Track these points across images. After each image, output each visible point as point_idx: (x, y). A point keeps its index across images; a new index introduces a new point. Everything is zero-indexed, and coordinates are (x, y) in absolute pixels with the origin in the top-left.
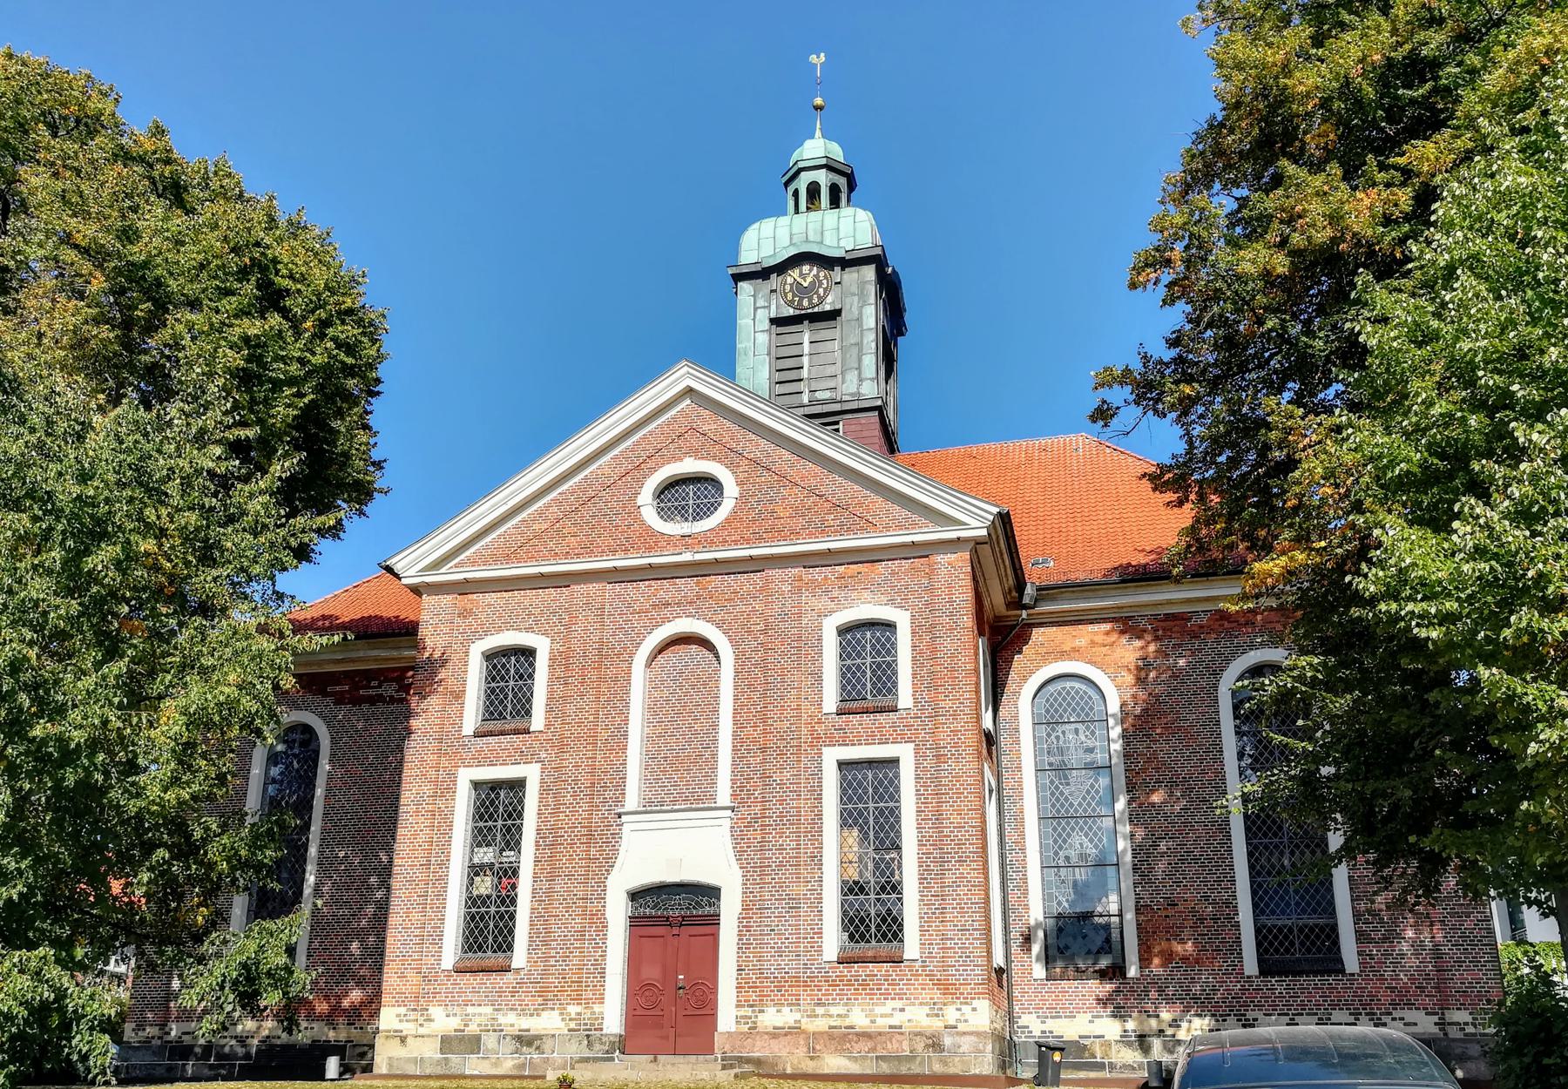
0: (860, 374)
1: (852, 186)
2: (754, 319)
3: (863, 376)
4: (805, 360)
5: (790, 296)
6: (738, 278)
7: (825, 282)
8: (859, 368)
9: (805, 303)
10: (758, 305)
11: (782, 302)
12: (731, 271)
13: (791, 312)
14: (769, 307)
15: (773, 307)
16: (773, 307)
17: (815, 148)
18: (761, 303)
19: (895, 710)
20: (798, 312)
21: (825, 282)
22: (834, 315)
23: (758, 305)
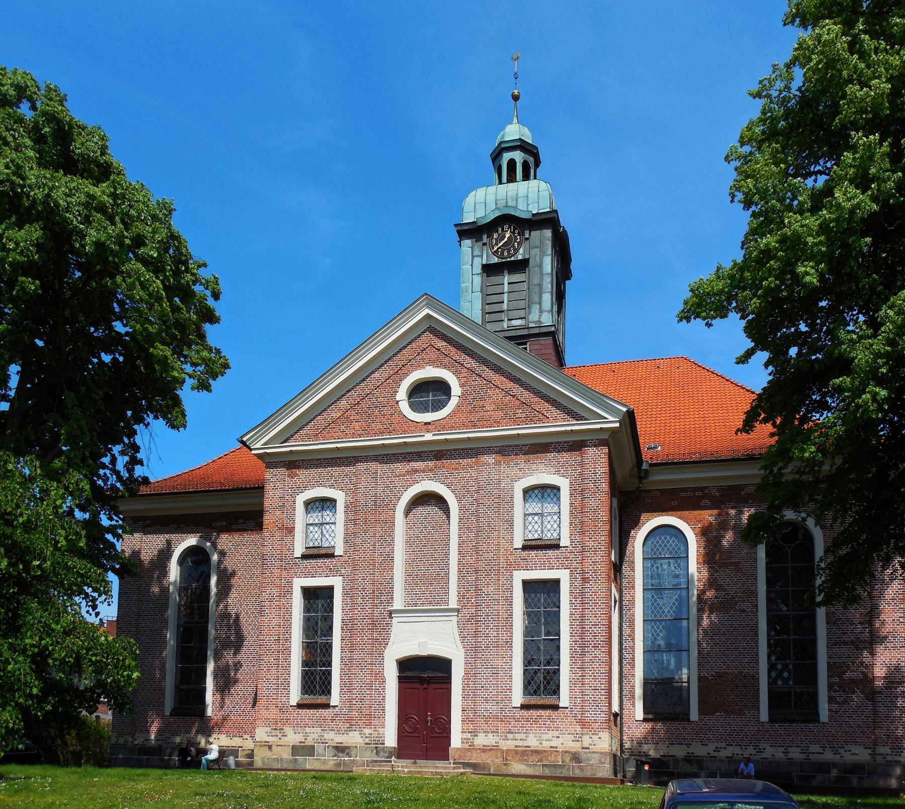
2: (472, 265)
9: (506, 254)
14: (482, 256)
15: (485, 256)
16: (485, 256)
23: (475, 254)
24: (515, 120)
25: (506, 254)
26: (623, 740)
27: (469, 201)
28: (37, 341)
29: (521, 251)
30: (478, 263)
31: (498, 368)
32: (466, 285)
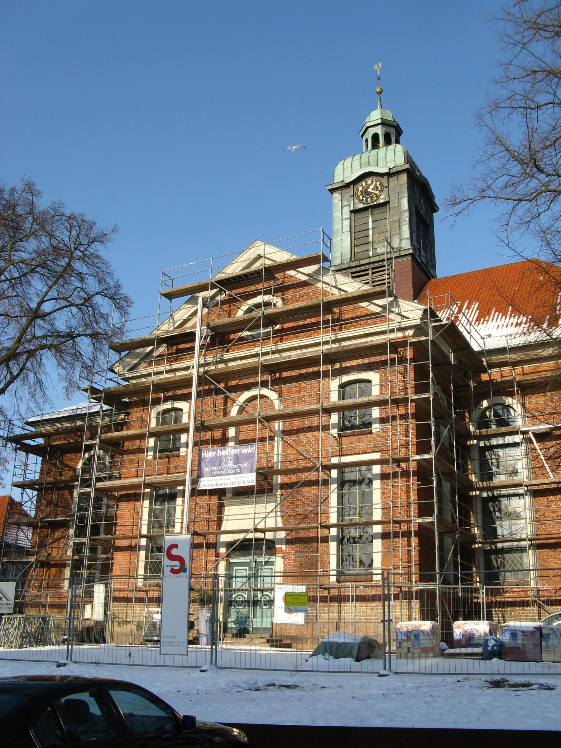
0: (400, 236)
1: (399, 132)
2: (342, 213)
3: (402, 237)
4: (370, 232)
5: (361, 198)
6: (332, 191)
7: (380, 187)
8: (400, 234)
9: (369, 200)
10: (344, 204)
11: (357, 201)
12: (330, 187)
13: (361, 206)
14: (350, 205)
15: (352, 205)
16: (352, 205)
17: (375, 116)
18: (345, 203)
19: (371, 433)
20: (365, 206)
21: (380, 187)
22: (385, 204)
23: (344, 204)
24: (379, 107)
25: (369, 200)
26: (497, 554)
27: (339, 169)
28: (124, 400)
29: (382, 197)
30: (346, 210)
31: (504, 674)
32: (337, 226)
